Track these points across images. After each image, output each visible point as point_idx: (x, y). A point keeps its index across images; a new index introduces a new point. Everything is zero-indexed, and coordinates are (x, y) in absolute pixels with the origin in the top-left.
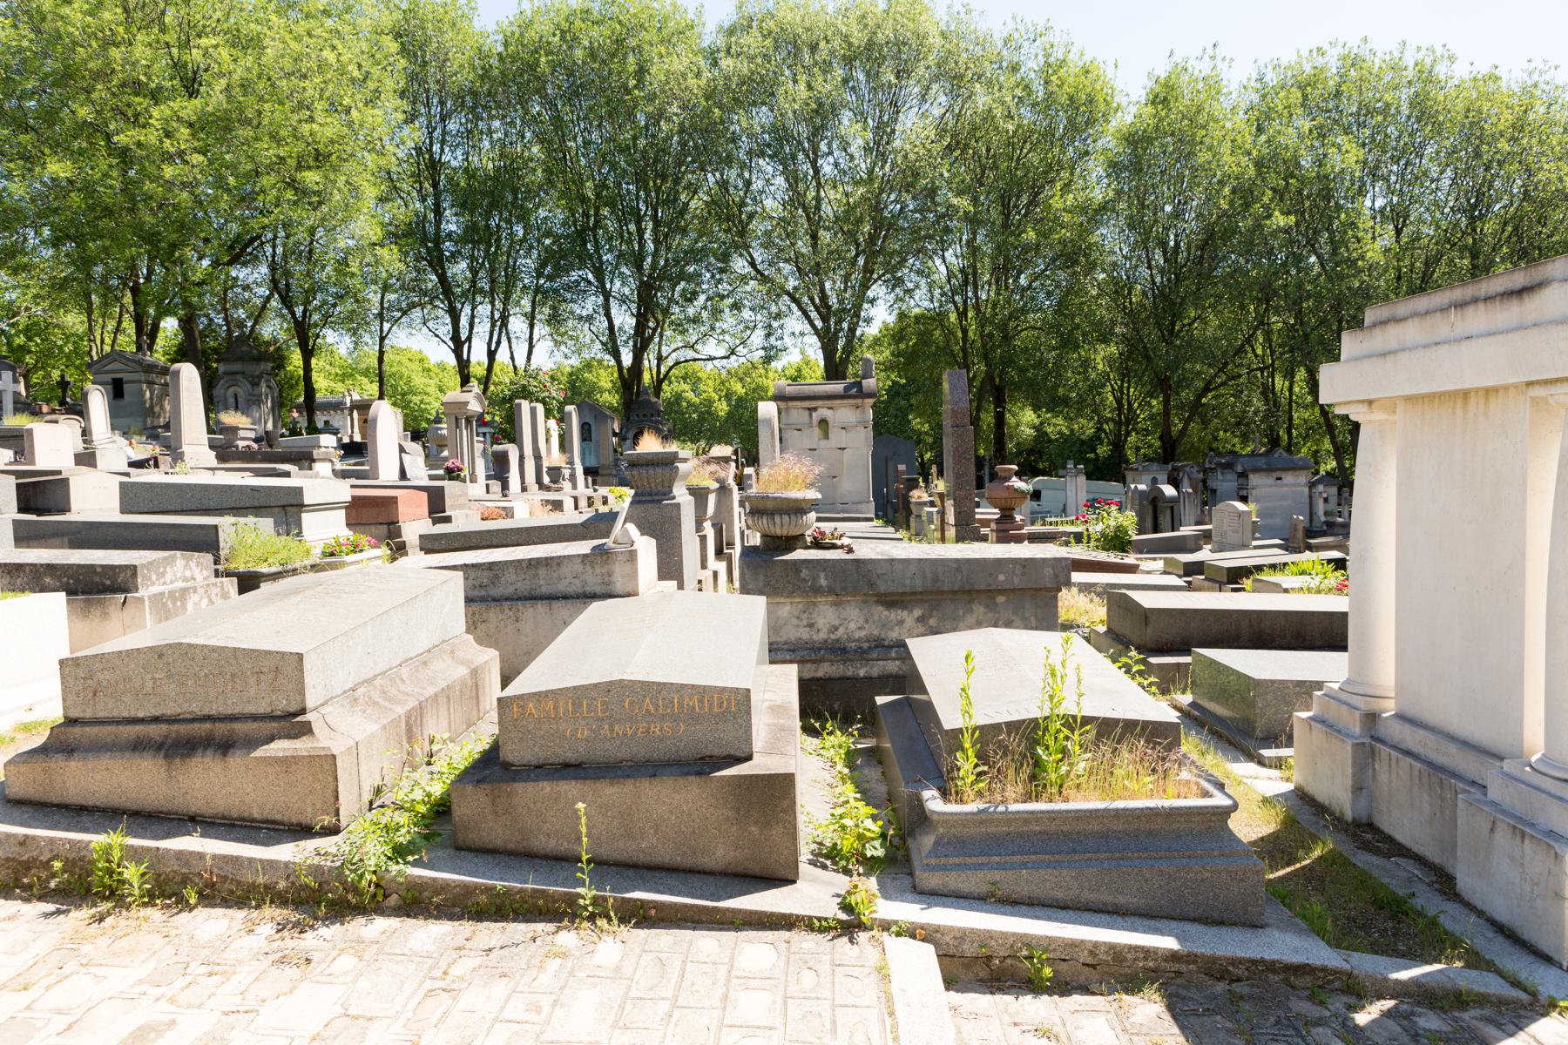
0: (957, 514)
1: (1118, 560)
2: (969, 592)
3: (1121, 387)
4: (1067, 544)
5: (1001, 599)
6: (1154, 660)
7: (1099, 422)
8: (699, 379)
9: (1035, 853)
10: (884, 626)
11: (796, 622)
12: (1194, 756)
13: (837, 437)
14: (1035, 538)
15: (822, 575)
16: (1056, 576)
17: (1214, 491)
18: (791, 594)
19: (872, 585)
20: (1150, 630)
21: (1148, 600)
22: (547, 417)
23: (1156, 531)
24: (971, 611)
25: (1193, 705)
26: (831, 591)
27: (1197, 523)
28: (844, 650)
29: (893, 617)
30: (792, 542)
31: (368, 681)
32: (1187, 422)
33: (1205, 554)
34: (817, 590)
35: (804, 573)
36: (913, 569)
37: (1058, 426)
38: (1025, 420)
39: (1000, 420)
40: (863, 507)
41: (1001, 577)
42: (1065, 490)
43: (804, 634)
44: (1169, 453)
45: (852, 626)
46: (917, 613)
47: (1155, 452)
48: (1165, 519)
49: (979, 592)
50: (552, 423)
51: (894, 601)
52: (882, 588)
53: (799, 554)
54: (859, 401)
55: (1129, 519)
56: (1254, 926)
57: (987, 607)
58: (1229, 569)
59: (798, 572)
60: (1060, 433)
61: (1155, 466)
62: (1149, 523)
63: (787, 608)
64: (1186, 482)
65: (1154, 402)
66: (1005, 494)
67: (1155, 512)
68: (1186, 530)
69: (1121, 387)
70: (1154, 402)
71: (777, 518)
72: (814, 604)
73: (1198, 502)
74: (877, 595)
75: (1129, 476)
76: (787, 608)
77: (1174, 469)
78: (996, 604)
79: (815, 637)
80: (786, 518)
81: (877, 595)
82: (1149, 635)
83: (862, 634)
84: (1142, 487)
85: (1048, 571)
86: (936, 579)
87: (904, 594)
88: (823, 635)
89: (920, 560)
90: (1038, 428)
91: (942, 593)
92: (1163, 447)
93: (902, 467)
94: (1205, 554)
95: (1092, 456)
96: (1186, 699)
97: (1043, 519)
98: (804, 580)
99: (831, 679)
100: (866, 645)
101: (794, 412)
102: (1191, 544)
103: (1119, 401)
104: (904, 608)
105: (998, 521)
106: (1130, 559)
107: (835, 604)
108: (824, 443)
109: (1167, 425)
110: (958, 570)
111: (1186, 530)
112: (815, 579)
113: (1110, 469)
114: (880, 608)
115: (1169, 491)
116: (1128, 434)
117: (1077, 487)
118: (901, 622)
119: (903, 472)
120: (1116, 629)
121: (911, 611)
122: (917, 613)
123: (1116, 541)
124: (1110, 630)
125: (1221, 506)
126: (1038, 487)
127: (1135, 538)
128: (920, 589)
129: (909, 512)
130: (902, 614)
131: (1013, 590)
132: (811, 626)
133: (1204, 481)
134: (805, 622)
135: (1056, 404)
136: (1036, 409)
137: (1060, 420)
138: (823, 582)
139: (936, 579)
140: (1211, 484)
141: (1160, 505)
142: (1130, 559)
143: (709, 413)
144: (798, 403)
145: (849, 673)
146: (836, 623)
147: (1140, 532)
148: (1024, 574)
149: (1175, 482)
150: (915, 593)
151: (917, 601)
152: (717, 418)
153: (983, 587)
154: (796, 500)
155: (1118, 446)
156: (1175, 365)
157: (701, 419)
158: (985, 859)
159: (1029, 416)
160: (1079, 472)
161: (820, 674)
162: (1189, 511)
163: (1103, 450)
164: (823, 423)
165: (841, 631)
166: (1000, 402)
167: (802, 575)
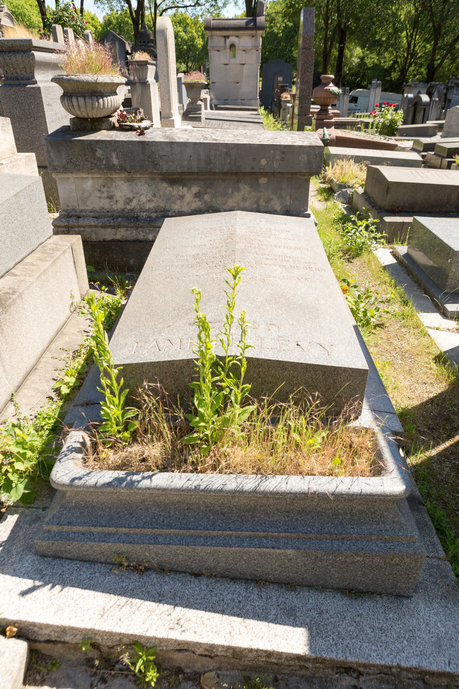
0: (300, 108)
1: (385, 141)
2: (237, 174)
3: (412, 35)
4: (359, 129)
5: (263, 181)
6: (388, 219)
7: (396, 57)
8: (188, 24)
9: (169, 526)
10: (168, 199)
11: (98, 194)
12: (291, 662)
13: (241, 57)
14: (339, 126)
15: (114, 155)
16: (309, 162)
17: (450, 100)
18: (90, 170)
19: (156, 165)
20: (389, 197)
21: (392, 174)
22: (76, 38)
23: (413, 123)
24: (238, 190)
25: (407, 255)
26: (122, 169)
27: (437, 119)
28: (137, 218)
29: (175, 192)
30: (97, 123)
31: (22, 191)
32: (444, 58)
33: (437, 139)
34: (111, 168)
35: (99, 153)
36: (189, 151)
37: (372, 59)
38: (355, 53)
39: (341, 51)
40: (253, 102)
41: (264, 162)
42: (369, 97)
43: (106, 204)
44: (431, 77)
45: (143, 199)
46: (195, 189)
47: (423, 77)
48: (419, 116)
49: (244, 173)
50: (80, 42)
51: (175, 179)
52: (164, 168)
53: (103, 135)
54: (254, 32)
55: (399, 116)
56: (399, 596)
57: (251, 186)
58: (450, 149)
59: (93, 151)
60: (373, 63)
61: (421, 84)
62: (410, 118)
63: (90, 182)
64: (436, 94)
65: (428, 46)
66: (324, 95)
67: (415, 112)
68: (430, 123)
69: (412, 35)
70: (428, 46)
71: (74, 100)
72: (112, 179)
73: (440, 106)
74: (161, 174)
75: (406, 89)
76: (90, 182)
77: (432, 87)
78: (258, 185)
79: (114, 207)
80: (81, 100)
81: (161, 174)
82: (387, 201)
83: (151, 205)
84: (411, 96)
85: (304, 158)
86: (208, 162)
87: (182, 173)
88: (120, 206)
89: (195, 144)
90: (362, 59)
91: (215, 174)
92: (428, 74)
93: (280, 79)
94: (437, 139)
95: (389, 78)
96: (402, 249)
97: (354, 113)
98: (99, 159)
99: (127, 241)
100: (154, 215)
101: (216, 38)
102: (431, 132)
103: (409, 44)
104: (184, 185)
105: (318, 113)
106: (392, 141)
107: (128, 180)
108: (232, 61)
109: (433, 60)
110: (227, 154)
111: (430, 123)
112: (108, 159)
113: (396, 87)
114: (165, 185)
115: (425, 98)
116: (410, 65)
117: (376, 94)
118: (182, 197)
119: (280, 82)
120: (369, 192)
121: (190, 188)
122: (195, 189)
123: (389, 130)
124: (365, 193)
125: (452, 109)
126: (356, 95)
127: (401, 127)
128: (195, 170)
129: (280, 107)
130: (183, 190)
131: (273, 174)
132: (111, 197)
133: (446, 95)
134: (105, 195)
135: (373, 45)
136: (363, 47)
137: (374, 56)
138: (115, 161)
139: (208, 162)
140: (450, 96)
141: (419, 107)
142: (392, 141)
143: (193, 45)
144: (218, 33)
145: (141, 237)
146: (131, 196)
147: (404, 123)
148: (282, 159)
149: (430, 94)
150: (192, 173)
151: (194, 179)
152: (197, 49)
153: (248, 170)
154: (88, 83)
155: (403, 71)
156: (444, 19)
157: (189, 50)
158: (112, 530)
159: (358, 51)
160: (378, 85)
161: (118, 237)
162: (433, 112)
163: (395, 75)
164: (232, 46)
165: (135, 202)
166: (342, 41)
167: (98, 154)
